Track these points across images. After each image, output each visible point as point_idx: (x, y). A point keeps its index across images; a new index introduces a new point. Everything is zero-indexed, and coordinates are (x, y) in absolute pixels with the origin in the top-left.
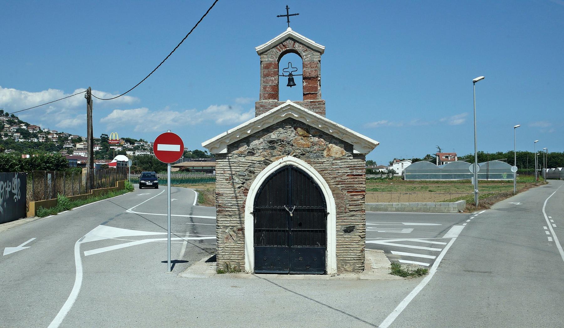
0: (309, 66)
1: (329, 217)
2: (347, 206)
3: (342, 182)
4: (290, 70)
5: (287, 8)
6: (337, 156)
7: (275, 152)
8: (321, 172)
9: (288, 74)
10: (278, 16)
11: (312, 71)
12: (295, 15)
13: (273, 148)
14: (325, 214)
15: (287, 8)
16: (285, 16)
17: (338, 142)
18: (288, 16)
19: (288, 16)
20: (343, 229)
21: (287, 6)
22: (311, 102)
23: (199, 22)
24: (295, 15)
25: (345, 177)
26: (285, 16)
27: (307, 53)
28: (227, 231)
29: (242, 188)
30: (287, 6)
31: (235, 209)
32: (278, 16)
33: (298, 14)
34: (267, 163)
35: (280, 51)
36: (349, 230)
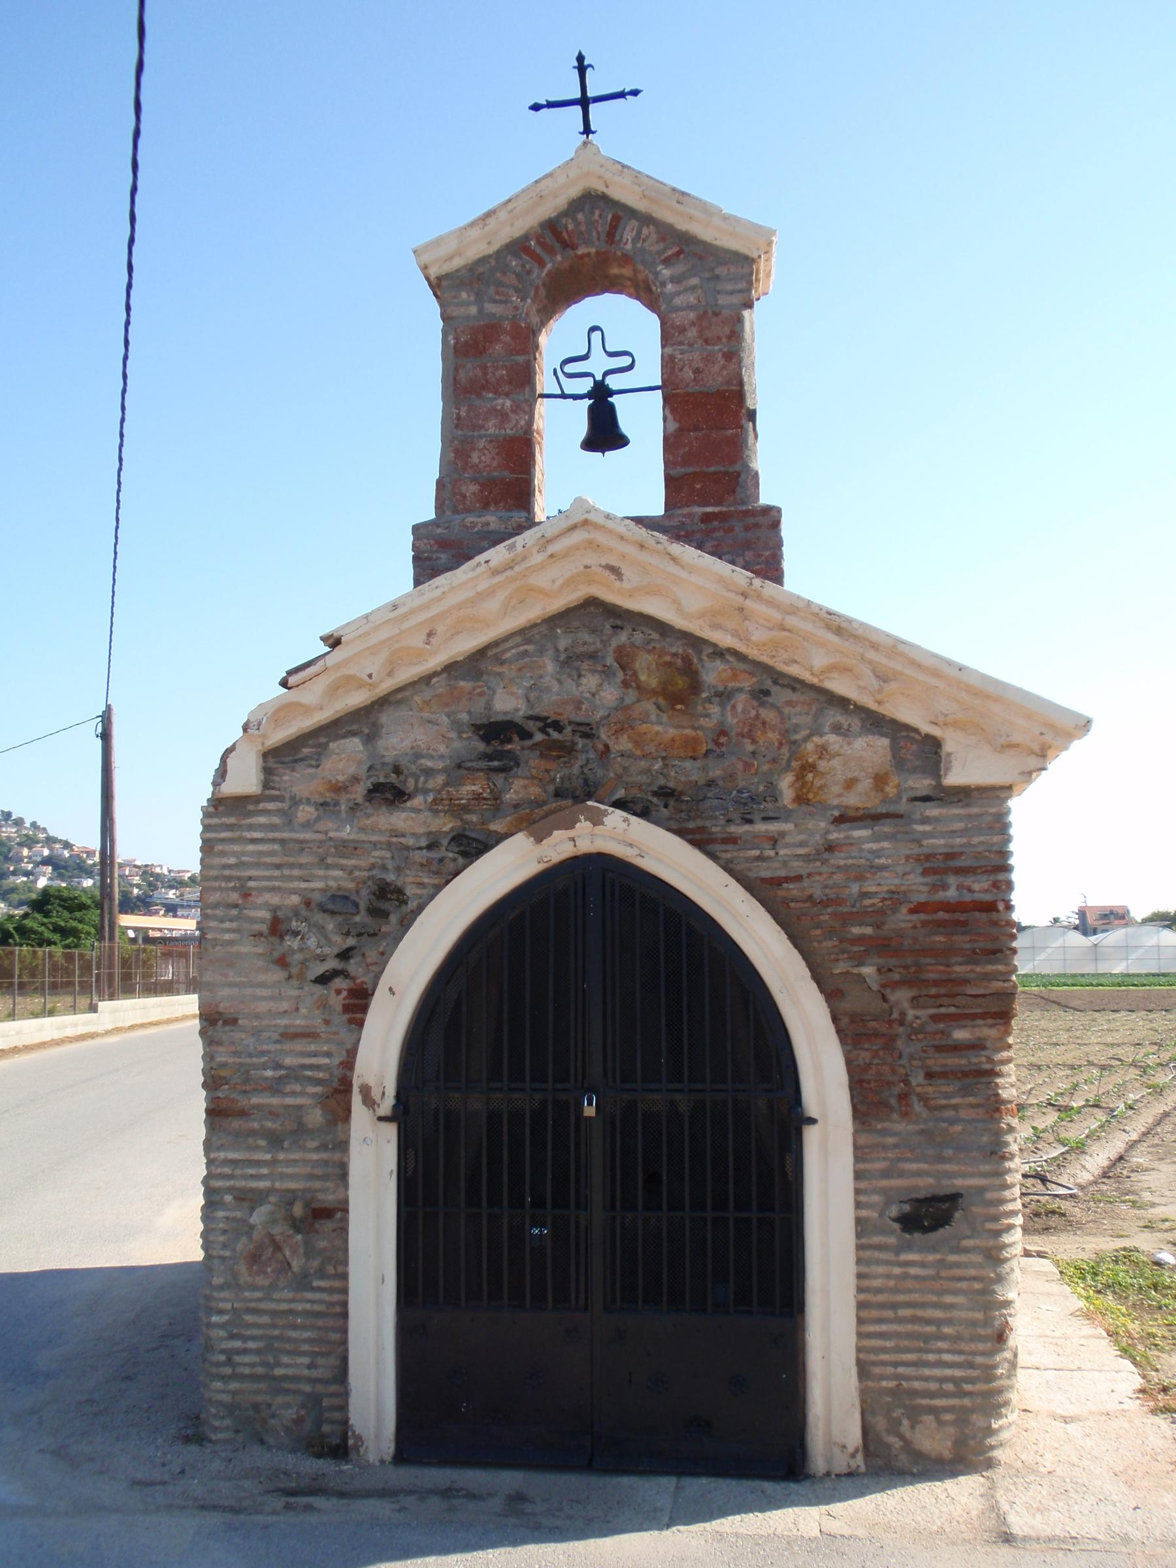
0: (692, 333)
1: (811, 1136)
2: (917, 1079)
3: (882, 946)
4: (598, 364)
5: (582, 68)
6: (853, 800)
7: (517, 789)
8: (764, 890)
9: (586, 385)
10: (536, 107)
11: (709, 359)
12: (621, 95)
13: (506, 765)
14: (790, 1121)
15: (582, 68)
16: (543, 396)
17: (856, 723)
18: (584, 102)
19: (584, 102)
20: (894, 1211)
21: (580, 58)
22: (707, 518)
23: (124, 391)
24: (621, 95)
25: (902, 919)
26: (543, 396)
27: (679, 269)
28: (257, 1218)
29: (339, 983)
30: (580, 58)
31: (304, 1099)
32: (536, 107)
33: (635, 93)
34: (472, 847)
35: (541, 263)
36: (928, 1215)
